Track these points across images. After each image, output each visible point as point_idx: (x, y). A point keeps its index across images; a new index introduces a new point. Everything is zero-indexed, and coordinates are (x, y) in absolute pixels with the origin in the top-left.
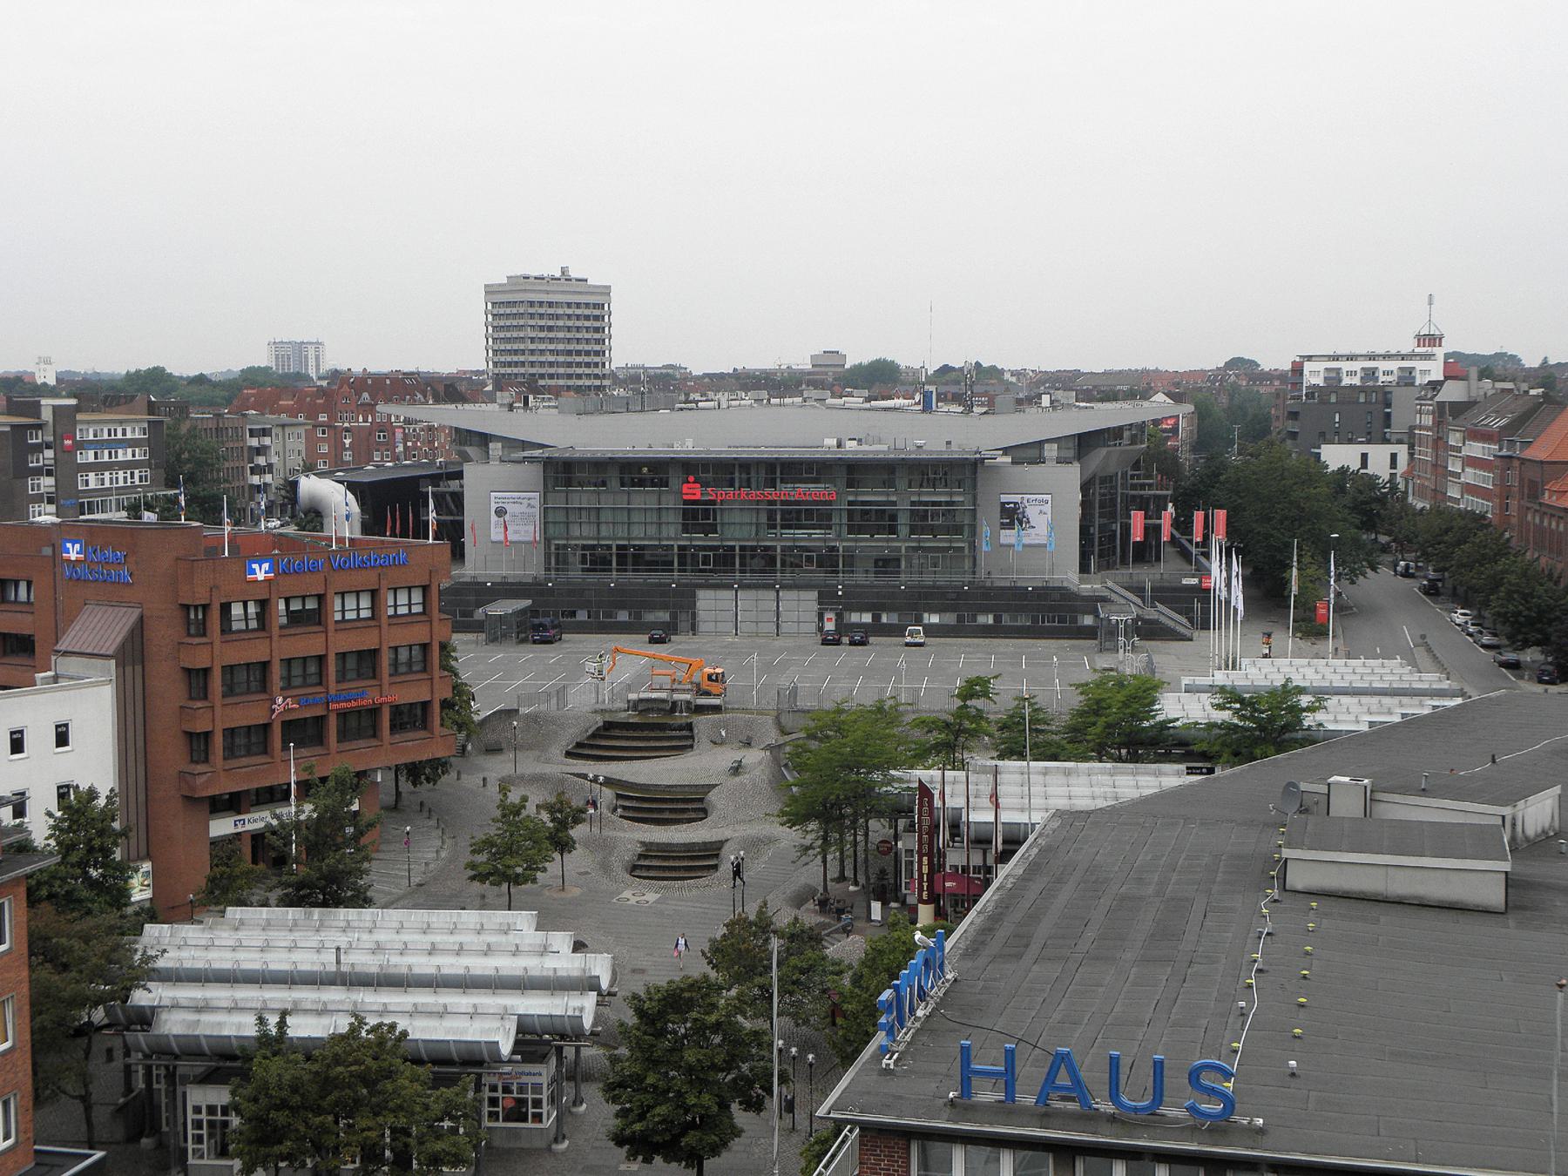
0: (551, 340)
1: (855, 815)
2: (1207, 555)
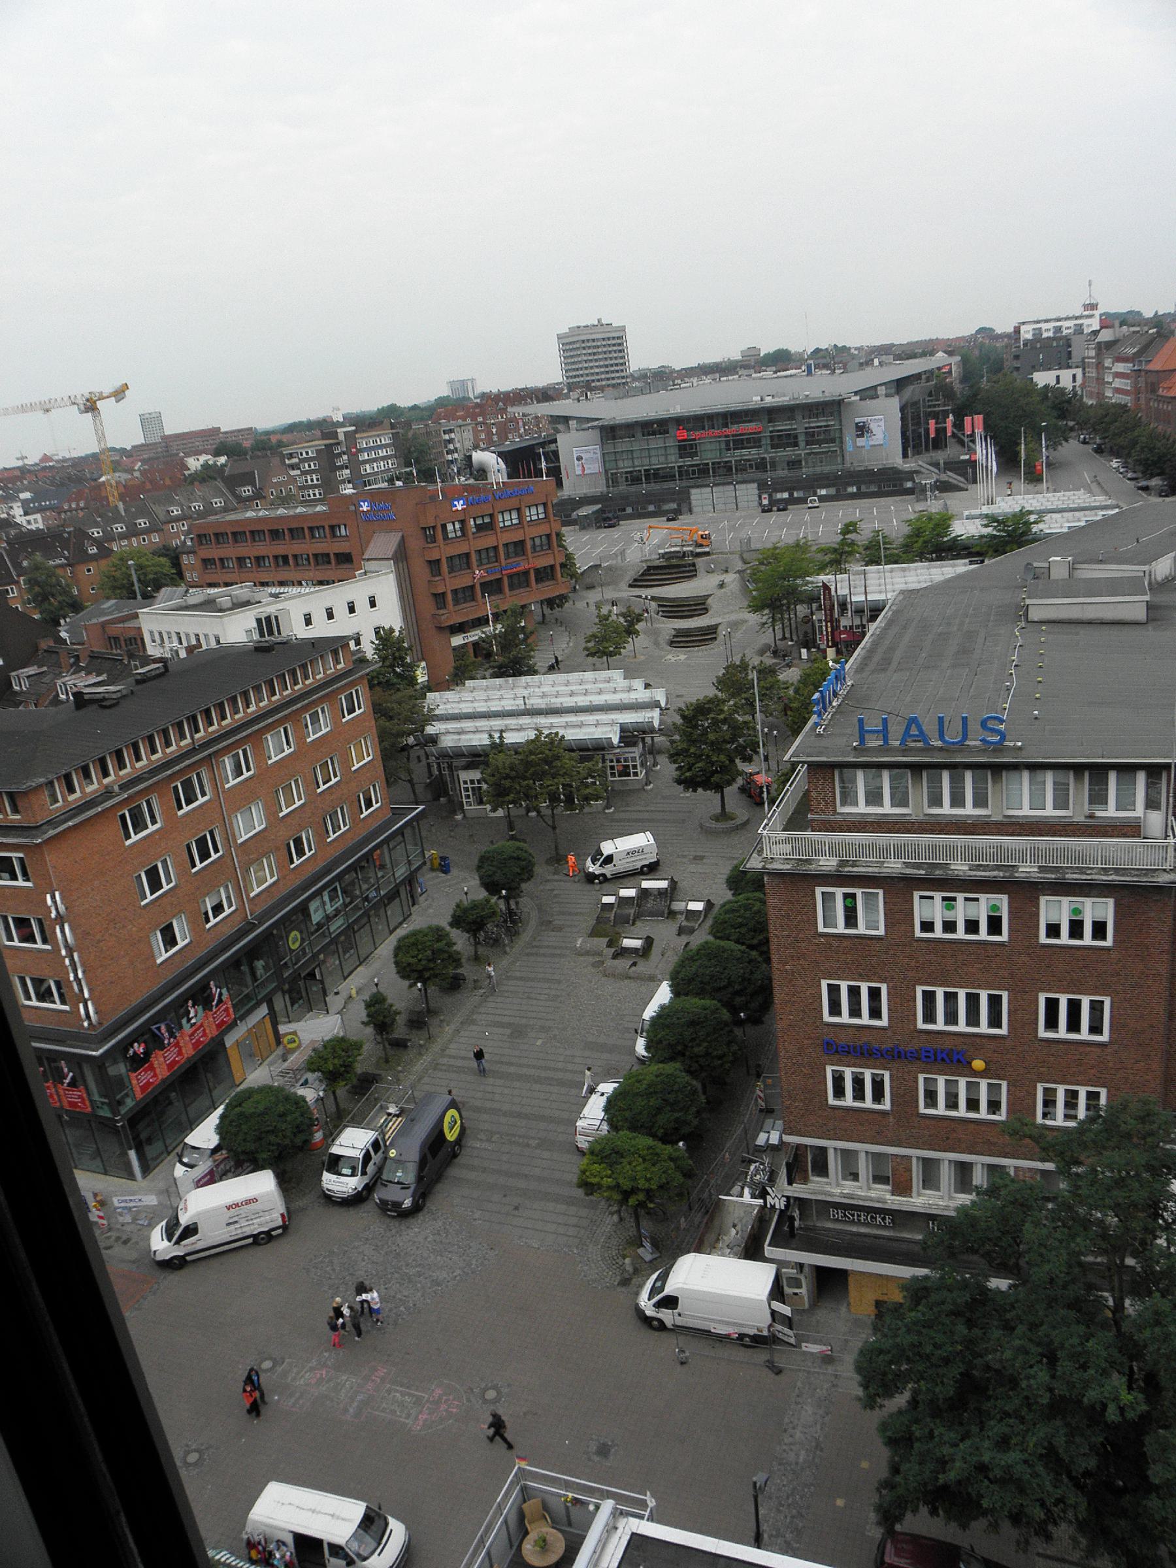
0: (596, 360)
1: (789, 604)
2: (973, 442)
